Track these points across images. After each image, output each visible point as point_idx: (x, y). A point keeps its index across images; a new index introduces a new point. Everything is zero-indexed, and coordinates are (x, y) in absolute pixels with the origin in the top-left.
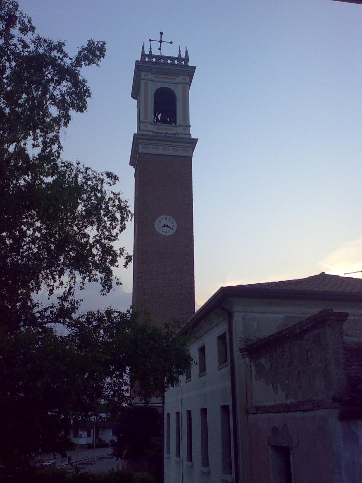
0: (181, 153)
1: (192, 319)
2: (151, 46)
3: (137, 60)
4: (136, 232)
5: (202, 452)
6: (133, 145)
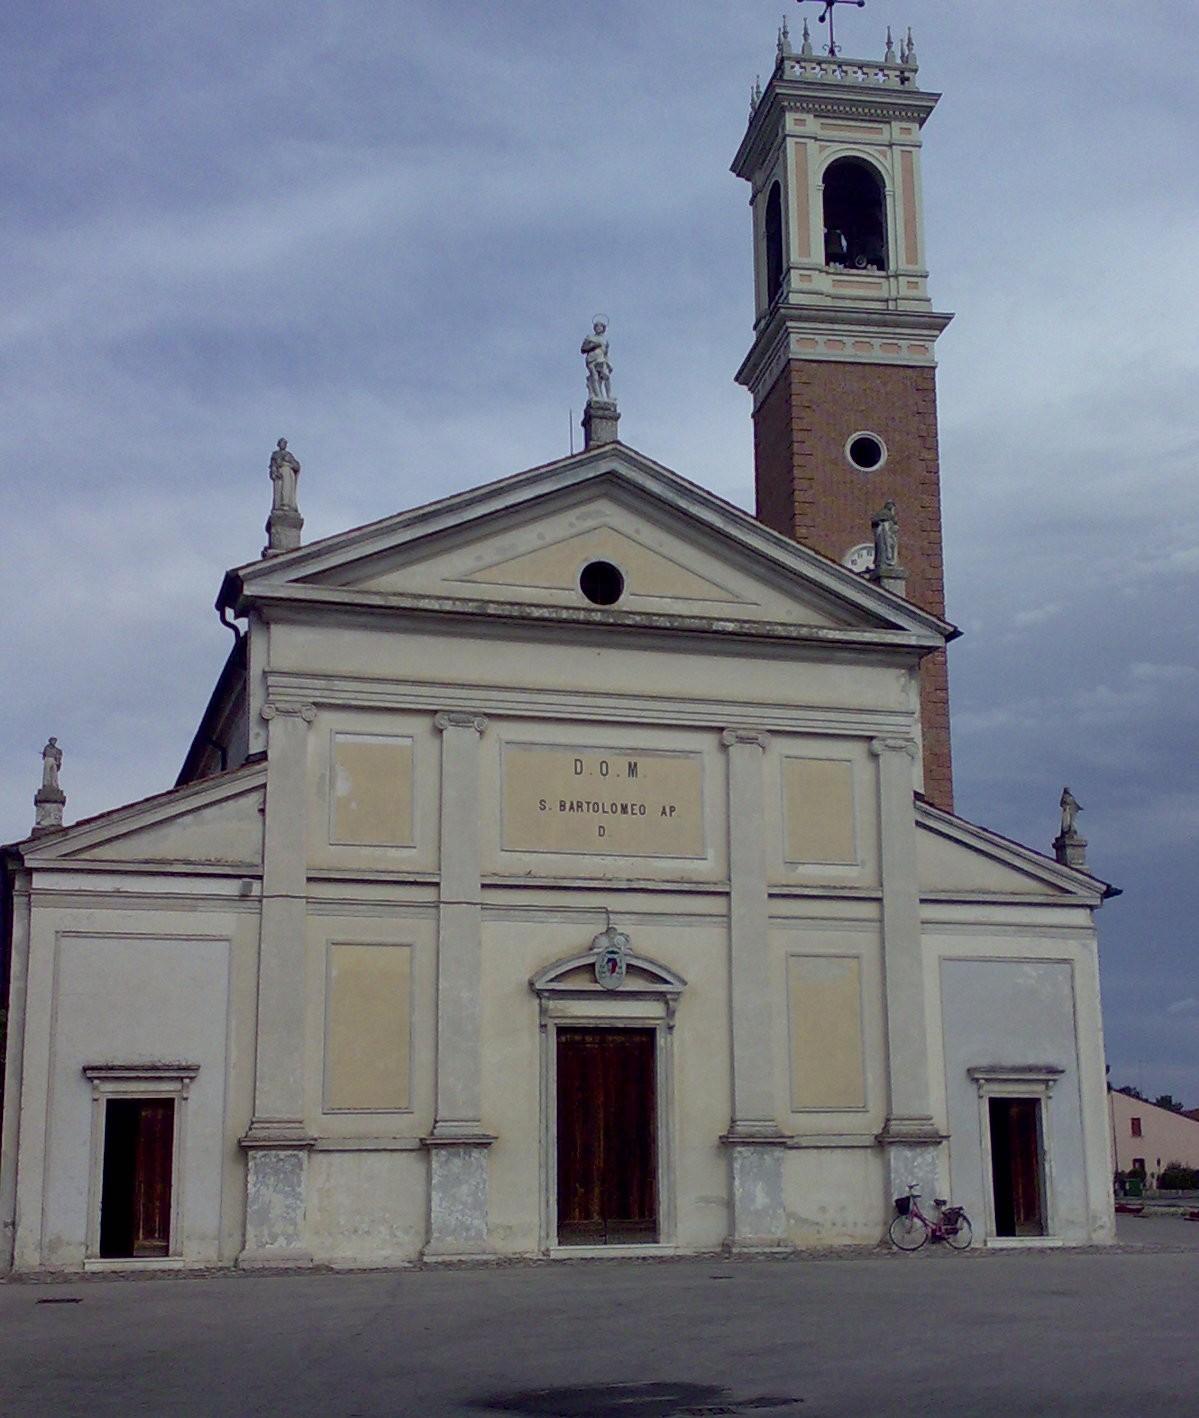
0: (905, 356)
1: (734, 1026)
2: (806, 29)
3: (730, 166)
4: (884, 230)
5: (582, 1259)
6: (745, 365)
